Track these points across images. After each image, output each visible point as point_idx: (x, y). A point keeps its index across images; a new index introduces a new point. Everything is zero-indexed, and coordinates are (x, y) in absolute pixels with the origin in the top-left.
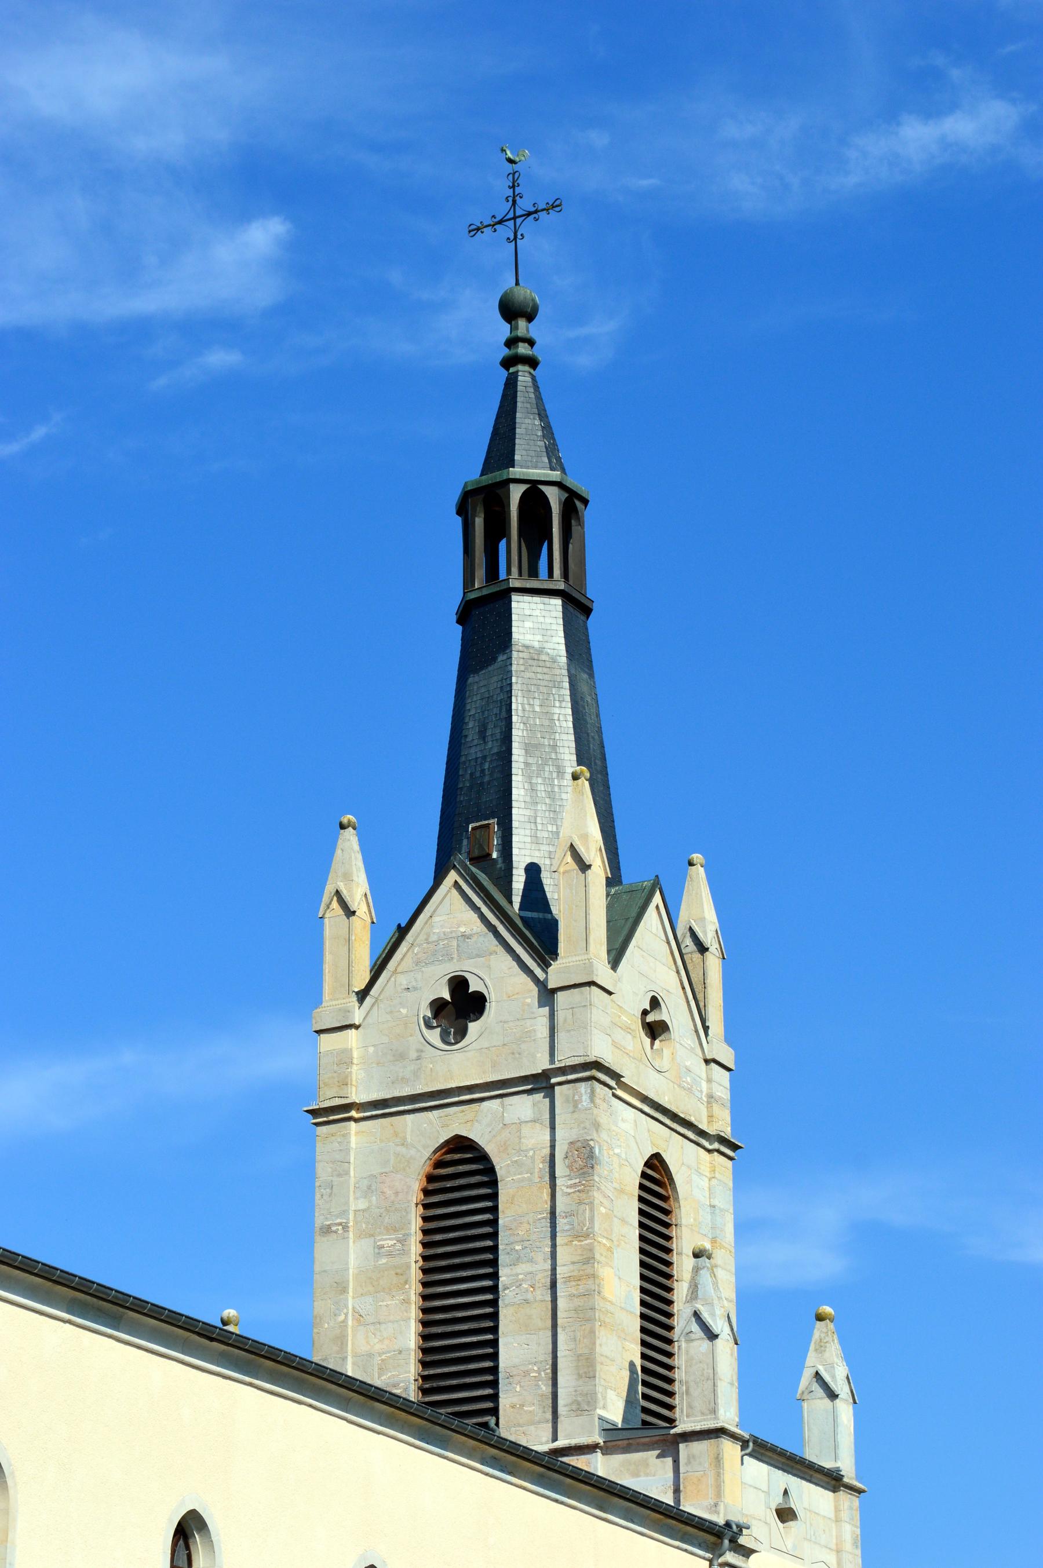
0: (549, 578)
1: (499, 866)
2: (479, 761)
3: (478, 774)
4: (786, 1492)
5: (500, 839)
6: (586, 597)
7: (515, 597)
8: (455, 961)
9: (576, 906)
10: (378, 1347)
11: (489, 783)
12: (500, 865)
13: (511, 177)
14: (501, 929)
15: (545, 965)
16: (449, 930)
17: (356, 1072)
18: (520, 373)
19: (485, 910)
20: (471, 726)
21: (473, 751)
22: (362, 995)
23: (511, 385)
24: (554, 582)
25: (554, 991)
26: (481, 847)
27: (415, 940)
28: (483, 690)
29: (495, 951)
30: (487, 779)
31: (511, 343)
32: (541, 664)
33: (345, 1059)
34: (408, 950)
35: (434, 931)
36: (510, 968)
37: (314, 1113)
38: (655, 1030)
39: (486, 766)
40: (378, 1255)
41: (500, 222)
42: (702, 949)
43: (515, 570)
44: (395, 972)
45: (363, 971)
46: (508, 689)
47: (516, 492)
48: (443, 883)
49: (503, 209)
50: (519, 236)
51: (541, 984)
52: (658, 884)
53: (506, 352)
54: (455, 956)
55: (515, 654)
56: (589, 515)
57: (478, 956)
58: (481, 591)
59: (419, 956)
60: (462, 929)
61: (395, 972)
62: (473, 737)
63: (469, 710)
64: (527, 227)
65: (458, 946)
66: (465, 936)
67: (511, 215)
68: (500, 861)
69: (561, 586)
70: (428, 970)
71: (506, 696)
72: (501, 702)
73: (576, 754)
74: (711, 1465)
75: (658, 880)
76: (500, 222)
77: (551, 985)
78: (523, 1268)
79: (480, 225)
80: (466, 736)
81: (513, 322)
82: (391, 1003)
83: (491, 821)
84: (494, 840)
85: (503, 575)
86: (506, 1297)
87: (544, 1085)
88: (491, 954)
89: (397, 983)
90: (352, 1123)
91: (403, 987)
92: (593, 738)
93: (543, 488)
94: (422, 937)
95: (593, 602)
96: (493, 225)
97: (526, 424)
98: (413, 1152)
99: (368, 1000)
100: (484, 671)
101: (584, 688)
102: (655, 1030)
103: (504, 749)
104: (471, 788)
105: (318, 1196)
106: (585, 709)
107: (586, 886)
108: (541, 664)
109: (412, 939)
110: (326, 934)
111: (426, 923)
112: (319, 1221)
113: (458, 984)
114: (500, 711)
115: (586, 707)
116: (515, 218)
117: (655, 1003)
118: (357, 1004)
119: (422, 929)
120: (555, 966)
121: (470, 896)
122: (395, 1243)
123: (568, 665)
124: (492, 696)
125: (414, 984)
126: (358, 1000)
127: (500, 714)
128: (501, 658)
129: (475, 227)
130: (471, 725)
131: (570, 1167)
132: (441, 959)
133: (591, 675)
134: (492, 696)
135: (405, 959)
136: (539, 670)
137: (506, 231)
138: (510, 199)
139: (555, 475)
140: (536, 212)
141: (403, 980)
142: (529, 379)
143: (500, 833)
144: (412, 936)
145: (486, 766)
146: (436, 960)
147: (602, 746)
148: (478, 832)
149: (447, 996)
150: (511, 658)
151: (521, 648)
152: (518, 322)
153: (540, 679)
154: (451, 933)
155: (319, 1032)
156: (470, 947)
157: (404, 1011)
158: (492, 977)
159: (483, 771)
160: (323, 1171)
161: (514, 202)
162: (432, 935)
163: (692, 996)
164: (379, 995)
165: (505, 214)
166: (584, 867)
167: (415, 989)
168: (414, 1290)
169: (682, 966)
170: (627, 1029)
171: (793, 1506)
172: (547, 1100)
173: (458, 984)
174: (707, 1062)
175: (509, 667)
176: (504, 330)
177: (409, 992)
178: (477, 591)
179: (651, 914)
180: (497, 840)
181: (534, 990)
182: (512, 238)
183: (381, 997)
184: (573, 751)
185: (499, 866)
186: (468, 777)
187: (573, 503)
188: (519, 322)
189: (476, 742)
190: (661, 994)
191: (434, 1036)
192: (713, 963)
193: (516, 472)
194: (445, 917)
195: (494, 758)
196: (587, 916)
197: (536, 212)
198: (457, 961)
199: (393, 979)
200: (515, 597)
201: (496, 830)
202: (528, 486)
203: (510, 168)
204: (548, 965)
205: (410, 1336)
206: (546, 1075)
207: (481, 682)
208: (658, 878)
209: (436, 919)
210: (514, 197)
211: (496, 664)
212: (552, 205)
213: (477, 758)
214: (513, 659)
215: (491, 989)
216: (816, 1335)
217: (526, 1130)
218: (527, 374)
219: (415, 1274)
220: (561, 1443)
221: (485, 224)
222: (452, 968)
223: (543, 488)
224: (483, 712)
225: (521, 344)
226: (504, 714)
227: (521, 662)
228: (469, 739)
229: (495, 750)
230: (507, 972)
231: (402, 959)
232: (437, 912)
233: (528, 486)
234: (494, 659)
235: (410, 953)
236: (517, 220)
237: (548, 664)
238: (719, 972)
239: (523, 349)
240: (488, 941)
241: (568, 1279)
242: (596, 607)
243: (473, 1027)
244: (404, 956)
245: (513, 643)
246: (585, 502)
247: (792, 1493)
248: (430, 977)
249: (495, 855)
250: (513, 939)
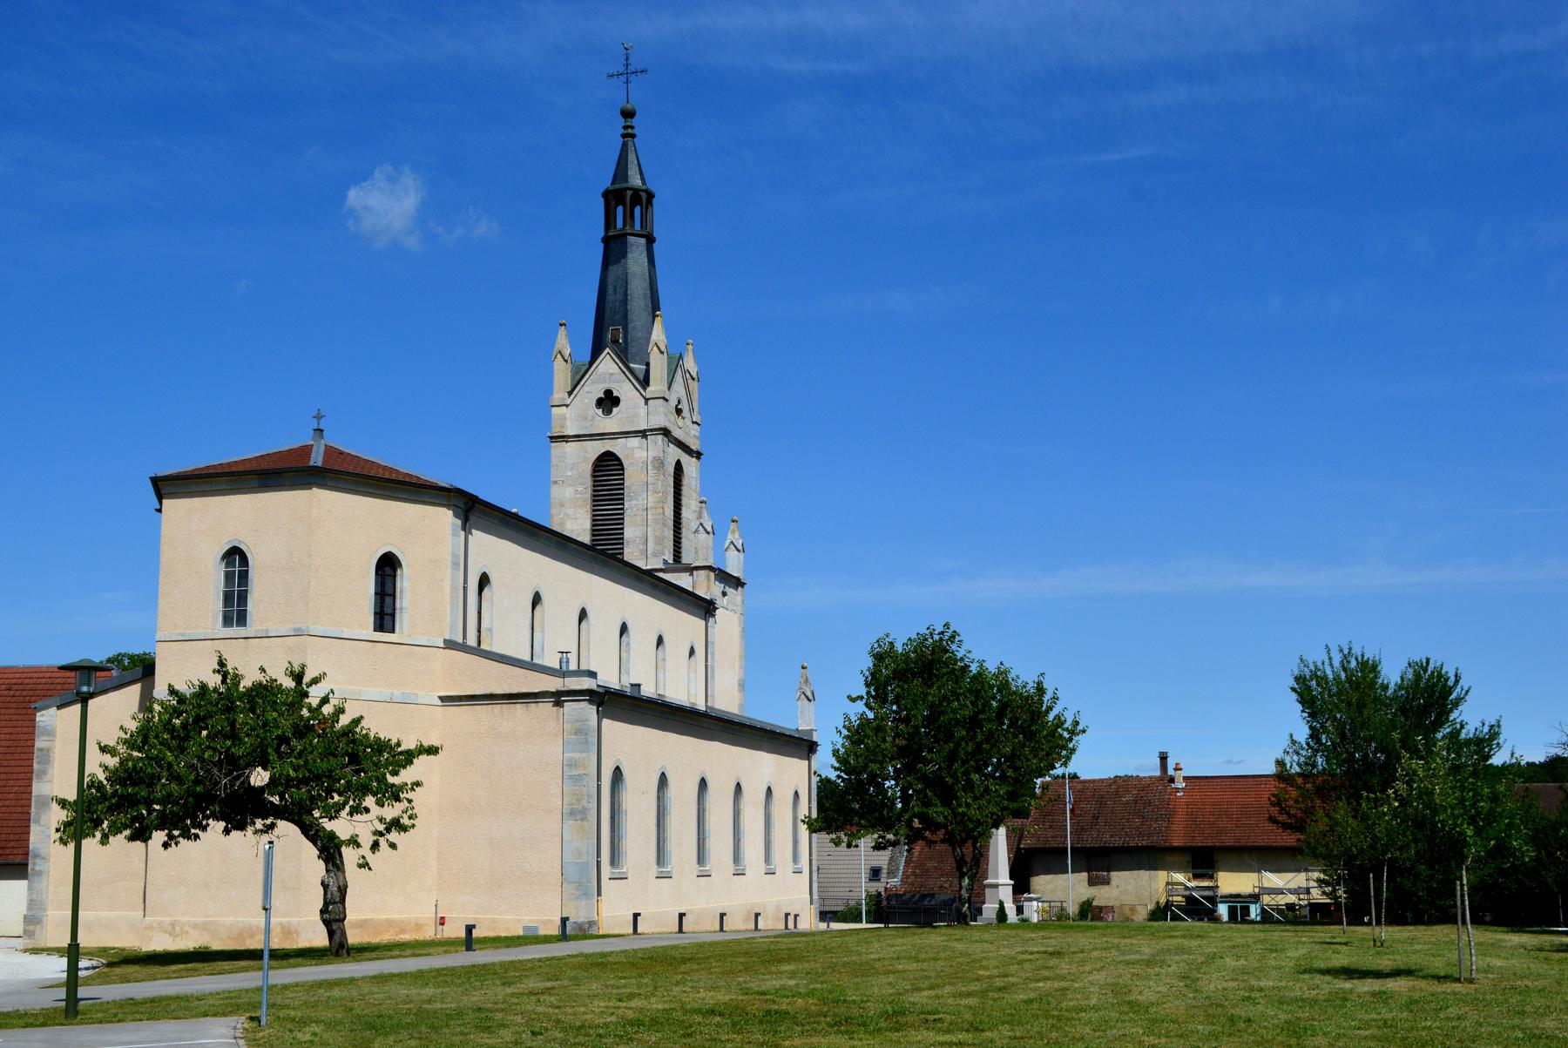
10: (576, 528)
14: (627, 373)
15: (645, 389)
17: (568, 423)
19: (620, 364)
20: (610, 289)
23: (624, 145)
31: (625, 128)
33: (563, 418)
37: (551, 438)
38: (679, 412)
40: (576, 493)
47: (629, 193)
53: (622, 131)
56: (655, 201)
64: (632, 78)
66: (612, 374)
70: (597, 386)
74: (1433, 995)
77: (647, 397)
78: (634, 502)
85: (619, 224)
86: (628, 513)
93: (641, 193)
97: (632, 158)
98: (590, 456)
99: (573, 396)
101: (652, 274)
102: (679, 412)
105: (552, 469)
112: (552, 479)
113: (608, 393)
116: (627, 74)
120: (649, 389)
122: (961, 709)
128: (623, 261)
131: (653, 466)
139: (644, 187)
155: (553, 406)
157: (586, 401)
160: (554, 460)
168: (588, 508)
170: (671, 413)
173: (608, 393)
176: (622, 121)
185: (1438, 902)
187: (651, 196)
191: (600, 412)
205: (587, 525)
207: (614, 271)
216: (732, 527)
217: (635, 451)
219: (589, 501)
223: (641, 193)
239: (630, 131)
241: (652, 508)
243: (615, 410)
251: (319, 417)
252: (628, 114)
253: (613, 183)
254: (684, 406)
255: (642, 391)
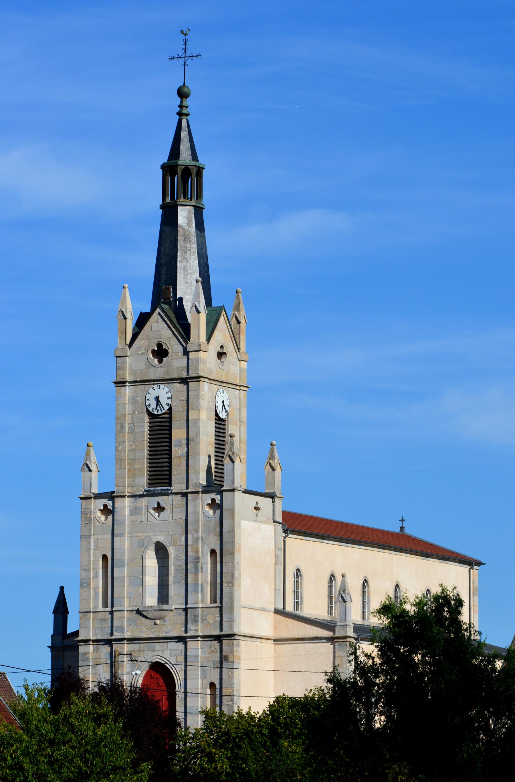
4: (257, 502)
13: (184, 41)
22: (130, 345)
56: (205, 173)
64: (189, 61)
87: (186, 381)
90: (127, 357)
93: (188, 167)
97: (184, 134)
113: (160, 345)
117: (222, 347)
118: (128, 349)
126: (129, 348)
149: (156, 349)
166: (199, 312)
171: (259, 506)
172: (219, 644)
173: (160, 345)
174: (239, 360)
176: (178, 100)
179: (222, 319)
181: (181, 349)
187: (200, 171)
202: (185, 166)
203: (183, 37)
204: (188, 343)
206: (186, 379)
223: (188, 167)
233: (185, 166)
236: (184, 56)
239: (184, 111)
247: (259, 503)
249: (171, 299)
251: (402, 520)
252: (182, 94)
253: (169, 159)
254: (230, 348)
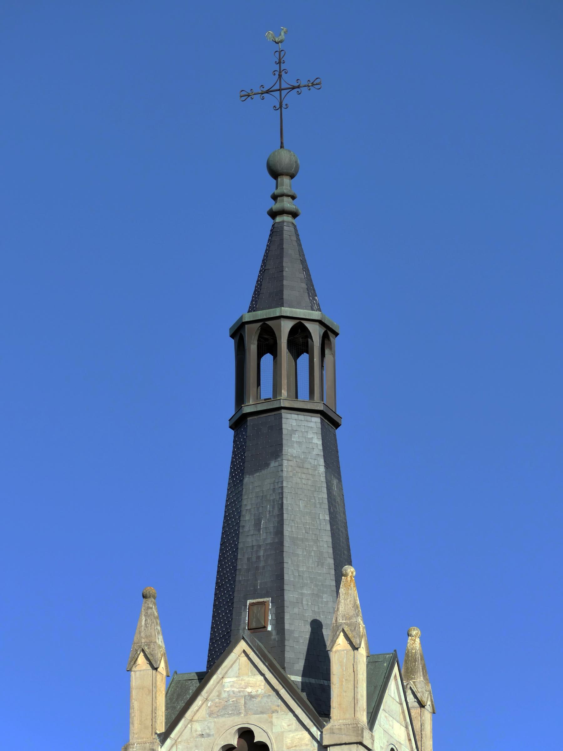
0: (310, 399)
1: (273, 637)
2: (255, 547)
3: (254, 559)
5: (274, 615)
6: (336, 414)
7: (284, 414)
8: (243, 715)
9: (346, 680)
11: (264, 568)
12: (274, 636)
14: (283, 692)
16: (237, 690)
18: (285, 224)
20: (247, 519)
21: (249, 539)
24: (315, 404)
25: (326, 747)
26: (258, 620)
27: (208, 696)
28: (258, 490)
29: (276, 710)
30: (262, 564)
32: (305, 471)
34: (202, 704)
35: (225, 690)
36: (289, 725)
39: (261, 553)
41: (268, 92)
42: (422, 705)
43: (284, 393)
44: (191, 721)
45: (161, 715)
46: (280, 491)
47: (286, 326)
48: (234, 651)
49: (270, 81)
50: (284, 106)
51: (319, 743)
52: (396, 657)
54: (243, 711)
55: (285, 463)
56: (336, 342)
57: (262, 713)
58: (256, 407)
59: (212, 709)
60: (249, 690)
61: (191, 721)
62: (249, 527)
63: (246, 505)
64: (291, 98)
65: (245, 703)
66: (251, 697)
67: (277, 87)
68: (274, 633)
69: (321, 407)
71: (278, 497)
72: (274, 502)
73: (332, 547)
75: (396, 655)
76: (268, 92)
79: (249, 92)
80: (243, 526)
81: (279, 179)
82: (188, 745)
83: (265, 600)
84: (268, 616)
88: (273, 712)
89: (193, 729)
91: (198, 733)
92: (342, 532)
94: (214, 693)
95: (341, 418)
96: (262, 94)
99: (168, 742)
100: (258, 474)
103: (277, 541)
104: (248, 570)
106: (337, 509)
107: (354, 672)
108: (305, 471)
109: (206, 695)
110: (132, 684)
111: (218, 683)
114: (273, 508)
115: (337, 506)
119: (215, 687)
120: (328, 726)
121: (256, 664)
123: (326, 472)
124: (266, 496)
125: (208, 731)
126: (160, 741)
127: (273, 511)
128: (273, 464)
129: (246, 93)
130: (247, 518)
132: (230, 712)
133: (340, 480)
134: (266, 496)
135: (200, 711)
136: (304, 476)
137: (273, 100)
138: (277, 73)
139: (316, 315)
140: (299, 87)
141: (198, 727)
142: (292, 229)
143: (274, 610)
144: (207, 693)
145: (261, 553)
146: (227, 713)
147: (347, 539)
148: (255, 608)
150: (282, 465)
151: (290, 458)
152: (283, 179)
153: (304, 484)
154: (239, 692)
156: (255, 705)
158: (274, 731)
159: (258, 557)
161: (280, 76)
162: (223, 692)
163: (415, 746)
164: (178, 738)
165: (272, 86)
167: (209, 735)
169: (410, 722)
175: (280, 473)
176: (270, 221)
177: (203, 738)
178: (252, 406)
180: (271, 616)
182: (278, 106)
183: (179, 740)
184: (331, 545)
185: (273, 637)
186: (245, 561)
188: (284, 179)
189: (252, 532)
190: (396, 746)
192: (427, 716)
193: (286, 311)
194: (234, 679)
195: (268, 548)
196: (355, 689)
197: (299, 87)
198: (244, 716)
199: (189, 726)
200: (284, 414)
201: (270, 608)
208: (396, 652)
209: (226, 680)
210: (280, 72)
211: (269, 469)
212: (312, 83)
213: (253, 546)
214: (284, 466)
215: (273, 741)
218: (291, 225)
220: (279, 71)
221: (255, 92)
222: (241, 722)
224: (258, 509)
225: (285, 199)
226: (276, 512)
227: (290, 469)
228: (246, 529)
229: (269, 541)
230: (287, 728)
231: (198, 711)
232: (226, 676)
234: (267, 465)
235: (204, 705)
237: (310, 472)
238: (431, 724)
239: (287, 204)
240: (271, 701)
242: (343, 422)
244: (199, 708)
245: (283, 453)
246: (336, 334)
248: (221, 727)
249: (269, 628)
250: (296, 705)
255: (314, 730)
